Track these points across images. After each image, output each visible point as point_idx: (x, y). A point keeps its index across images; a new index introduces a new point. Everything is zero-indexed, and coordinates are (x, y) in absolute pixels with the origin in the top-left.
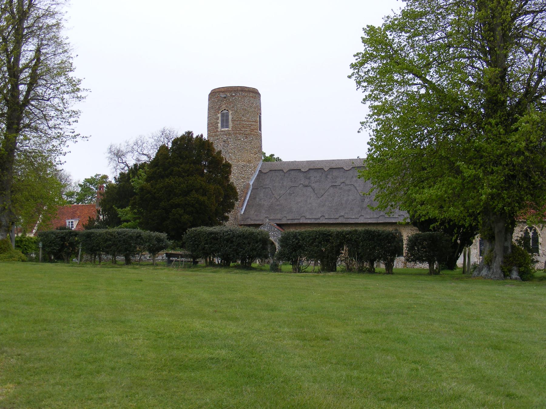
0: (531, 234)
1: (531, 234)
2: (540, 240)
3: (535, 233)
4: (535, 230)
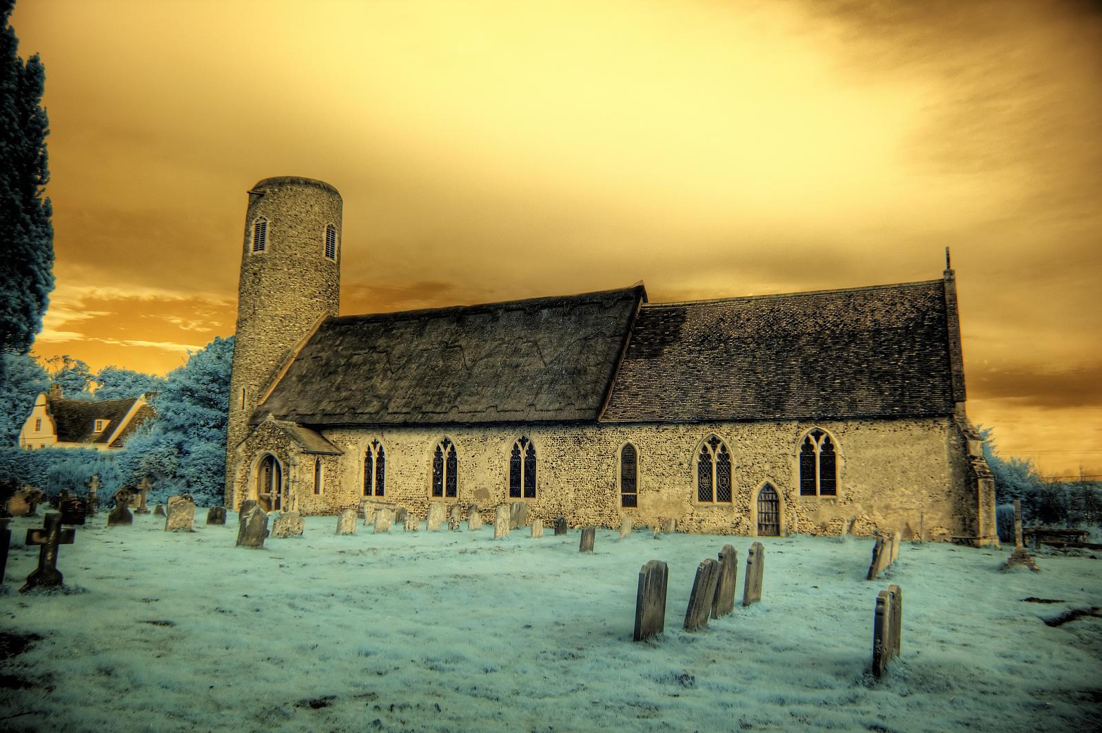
0: (818, 450)
1: (818, 450)
2: (840, 463)
3: (828, 447)
4: (828, 439)
